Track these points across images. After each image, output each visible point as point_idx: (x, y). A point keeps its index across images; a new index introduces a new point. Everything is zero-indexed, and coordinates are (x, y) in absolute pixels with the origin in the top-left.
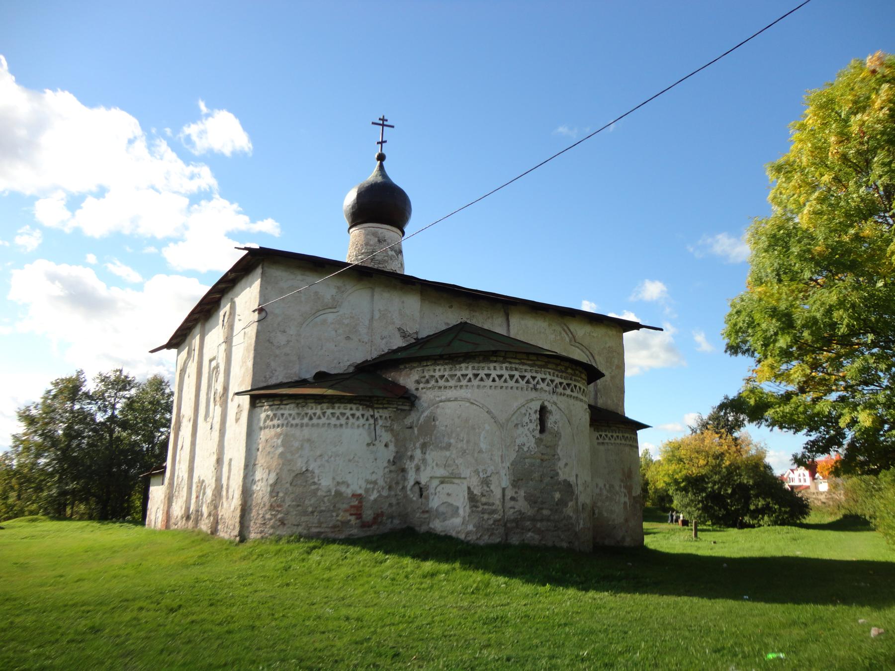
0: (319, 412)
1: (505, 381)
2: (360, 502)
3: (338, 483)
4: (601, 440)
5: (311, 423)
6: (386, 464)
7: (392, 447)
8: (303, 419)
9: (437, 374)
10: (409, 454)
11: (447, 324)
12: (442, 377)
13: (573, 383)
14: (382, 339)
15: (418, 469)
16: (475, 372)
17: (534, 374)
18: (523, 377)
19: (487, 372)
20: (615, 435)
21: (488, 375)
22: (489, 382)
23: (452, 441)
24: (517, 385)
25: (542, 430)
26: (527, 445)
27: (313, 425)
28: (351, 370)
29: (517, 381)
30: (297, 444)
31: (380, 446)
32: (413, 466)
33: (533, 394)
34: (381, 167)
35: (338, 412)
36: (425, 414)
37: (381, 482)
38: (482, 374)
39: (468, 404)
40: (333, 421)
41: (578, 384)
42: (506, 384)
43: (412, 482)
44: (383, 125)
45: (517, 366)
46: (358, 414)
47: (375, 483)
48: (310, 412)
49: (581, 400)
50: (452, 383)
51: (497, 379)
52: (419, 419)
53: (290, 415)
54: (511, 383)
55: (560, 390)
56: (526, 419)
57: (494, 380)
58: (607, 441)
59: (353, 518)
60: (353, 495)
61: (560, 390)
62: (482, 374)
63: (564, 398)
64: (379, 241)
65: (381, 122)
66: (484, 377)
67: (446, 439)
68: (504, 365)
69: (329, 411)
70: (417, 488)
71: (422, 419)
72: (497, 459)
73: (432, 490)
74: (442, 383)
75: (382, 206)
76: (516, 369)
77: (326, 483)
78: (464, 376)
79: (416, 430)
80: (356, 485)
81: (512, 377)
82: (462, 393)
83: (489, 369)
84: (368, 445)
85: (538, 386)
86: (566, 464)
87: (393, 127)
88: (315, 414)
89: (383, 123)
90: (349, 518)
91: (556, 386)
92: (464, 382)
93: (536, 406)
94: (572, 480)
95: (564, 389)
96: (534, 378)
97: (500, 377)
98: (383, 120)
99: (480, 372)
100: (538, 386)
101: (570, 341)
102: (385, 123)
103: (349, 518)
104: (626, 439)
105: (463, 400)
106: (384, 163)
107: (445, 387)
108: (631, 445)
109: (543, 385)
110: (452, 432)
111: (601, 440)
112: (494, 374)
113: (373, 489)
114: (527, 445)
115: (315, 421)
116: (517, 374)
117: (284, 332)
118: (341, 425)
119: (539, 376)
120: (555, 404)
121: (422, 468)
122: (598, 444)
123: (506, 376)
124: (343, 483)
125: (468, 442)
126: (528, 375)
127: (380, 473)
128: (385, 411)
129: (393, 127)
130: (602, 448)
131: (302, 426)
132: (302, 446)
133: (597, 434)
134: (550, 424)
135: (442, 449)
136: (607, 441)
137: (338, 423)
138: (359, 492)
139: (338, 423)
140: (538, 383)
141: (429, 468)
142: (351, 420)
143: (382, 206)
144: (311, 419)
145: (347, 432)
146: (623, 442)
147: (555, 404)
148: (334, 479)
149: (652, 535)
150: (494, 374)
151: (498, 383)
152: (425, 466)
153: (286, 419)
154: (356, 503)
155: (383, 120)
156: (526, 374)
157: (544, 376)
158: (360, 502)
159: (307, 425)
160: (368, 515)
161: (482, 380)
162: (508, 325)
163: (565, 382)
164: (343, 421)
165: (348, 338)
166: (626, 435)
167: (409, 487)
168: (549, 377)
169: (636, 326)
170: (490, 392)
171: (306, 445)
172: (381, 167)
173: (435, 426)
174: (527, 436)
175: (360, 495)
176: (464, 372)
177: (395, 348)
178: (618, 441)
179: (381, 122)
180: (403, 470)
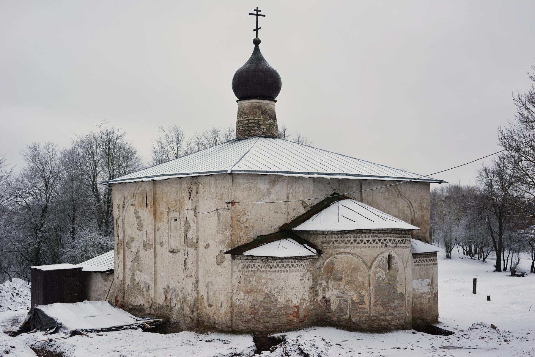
0: (275, 264)
1: (371, 243)
2: (298, 310)
3: (287, 301)
4: (417, 263)
5: (271, 270)
6: (309, 289)
7: (311, 280)
8: (266, 268)
9: (334, 239)
10: (319, 282)
11: (327, 195)
12: (336, 241)
13: (404, 239)
14: (293, 210)
15: (324, 290)
16: (355, 239)
17: (385, 238)
18: (379, 240)
19: (361, 238)
20: (425, 259)
21: (362, 241)
22: (362, 244)
23: (343, 276)
24: (377, 245)
25: (389, 268)
26: (382, 277)
27: (273, 272)
28: (277, 230)
29: (377, 243)
30: (264, 281)
31: (306, 280)
32: (321, 288)
33: (384, 249)
34: (257, 50)
35: (285, 264)
36: (327, 261)
37: (307, 299)
38: (359, 240)
39: (351, 256)
40: (283, 269)
41: (407, 239)
42: (371, 245)
43: (321, 297)
44: (257, 15)
45: (377, 235)
46: (295, 264)
47: (304, 299)
48: (271, 264)
49: (406, 247)
50: (342, 245)
51: (366, 242)
52: (323, 264)
53: (259, 266)
54: (374, 244)
55: (398, 245)
56: (381, 263)
57: (365, 243)
58: (420, 263)
59: (295, 318)
60: (294, 306)
61: (398, 245)
62: (359, 240)
63: (400, 249)
64: (262, 113)
65: (255, 13)
66: (360, 241)
67: (339, 275)
68: (370, 235)
69: (280, 264)
70: (323, 301)
71: (325, 264)
72: (367, 285)
73: (332, 301)
74: (336, 244)
75: (257, 83)
76: (376, 237)
77: (281, 300)
78: (349, 241)
79: (322, 269)
80: (296, 302)
81: (374, 241)
82: (348, 250)
83: (362, 237)
84: (300, 280)
85: (388, 245)
86: (401, 285)
87: (264, 16)
88: (273, 266)
89: (257, 13)
90: (294, 318)
91: (396, 243)
92: (349, 244)
93: (386, 255)
94: (404, 292)
95: (400, 243)
96: (385, 240)
97: (368, 241)
98: (257, 10)
99: (357, 239)
100: (388, 245)
101: (398, 195)
102: (259, 13)
103: (294, 318)
104: (430, 260)
105: (349, 253)
106: (260, 46)
107: (339, 247)
108: (434, 264)
109: (390, 244)
110: (343, 271)
111: (417, 263)
112: (365, 240)
113: (304, 302)
114: (382, 277)
115: (273, 269)
116: (377, 239)
117: (245, 214)
118: (287, 271)
119: (388, 239)
120: (396, 253)
121: (327, 290)
122: (415, 265)
123: (371, 241)
124: (290, 300)
125: (351, 276)
126: (382, 239)
127: (307, 294)
128: (307, 261)
129: (264, 16)
130: (417, 267)
131: (266, 272)
132: (267, 282)
133: (415, 260)
134: (393, 266)
135: (338, 280)
136: (420, 263)
137: (285, 270)
138: (298, 304)
139: (285, 270)
140: (387, 243)
141: (330, 291)
142: (292, 268)
143: (257, 83)
144: (271, 268)
145: (290, 274)
146: (429, 263)
147: (396, 253)
148: (285, 299)
149: (443, 337)
150: (365, 240)
151: (367, 244)
152: (328, 289)
153: (257, 267)
154: (296, 310)
155: (257, 10)
156: (381, 238)
157: (390, 238)
158: (298, 310)
159: (270, 271)
160: (301, 315)
161: (358, 243)
162: (361, 194)
163: (400, 239)
164: (288, 269)
165: (275, 212)
166: (431, 258)
167: (319, 300)
168: (393, 238)
169: (13, 168)
170: (362, 249)
171: (269, 282)
172: (257, 50)
173: (333, 268)
174: (382, 274)
175: (298, 306)
176: (349, 239)
177: (300, 215)
178: (426, 263)
179: (255, 13)
180: (316, 291)
